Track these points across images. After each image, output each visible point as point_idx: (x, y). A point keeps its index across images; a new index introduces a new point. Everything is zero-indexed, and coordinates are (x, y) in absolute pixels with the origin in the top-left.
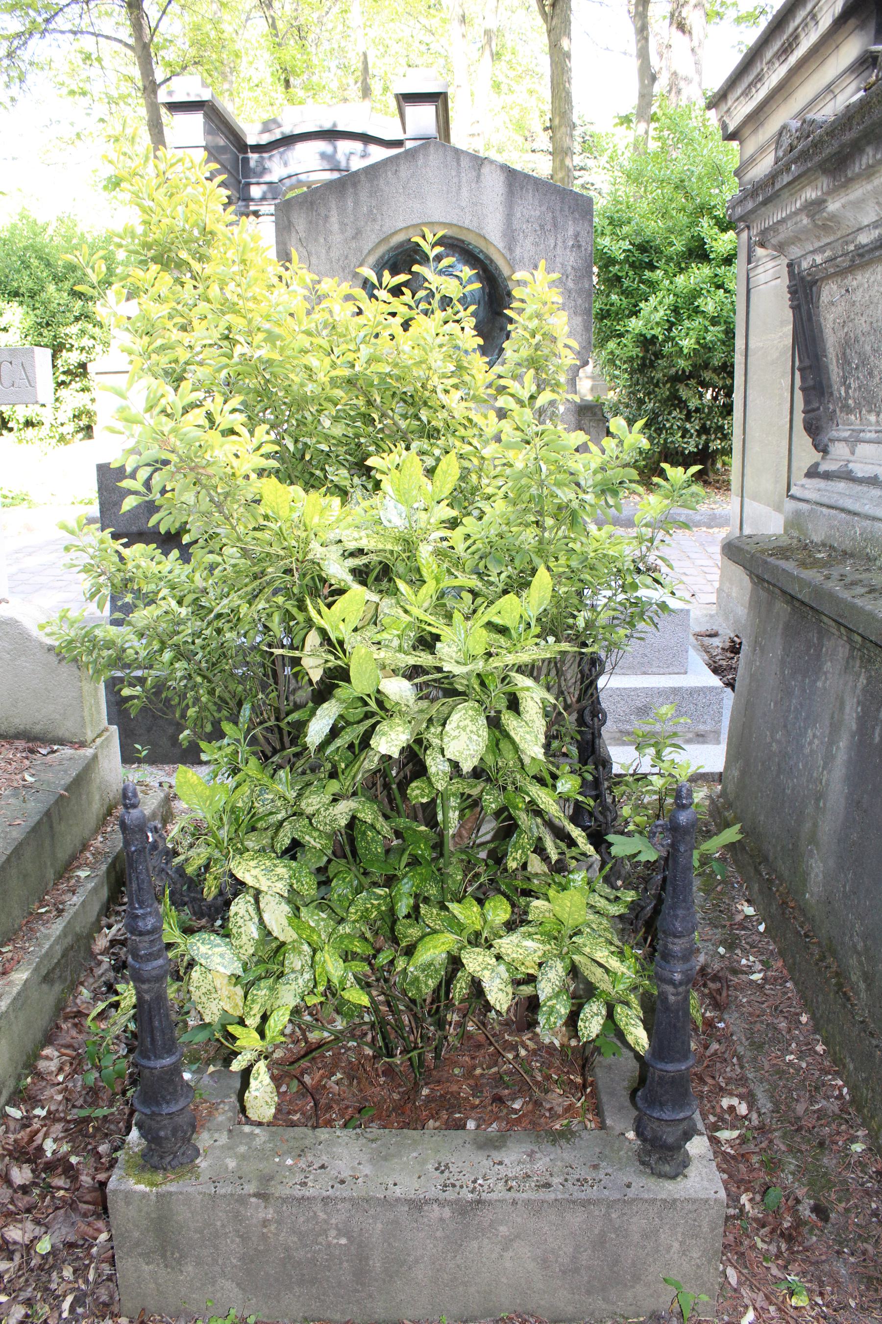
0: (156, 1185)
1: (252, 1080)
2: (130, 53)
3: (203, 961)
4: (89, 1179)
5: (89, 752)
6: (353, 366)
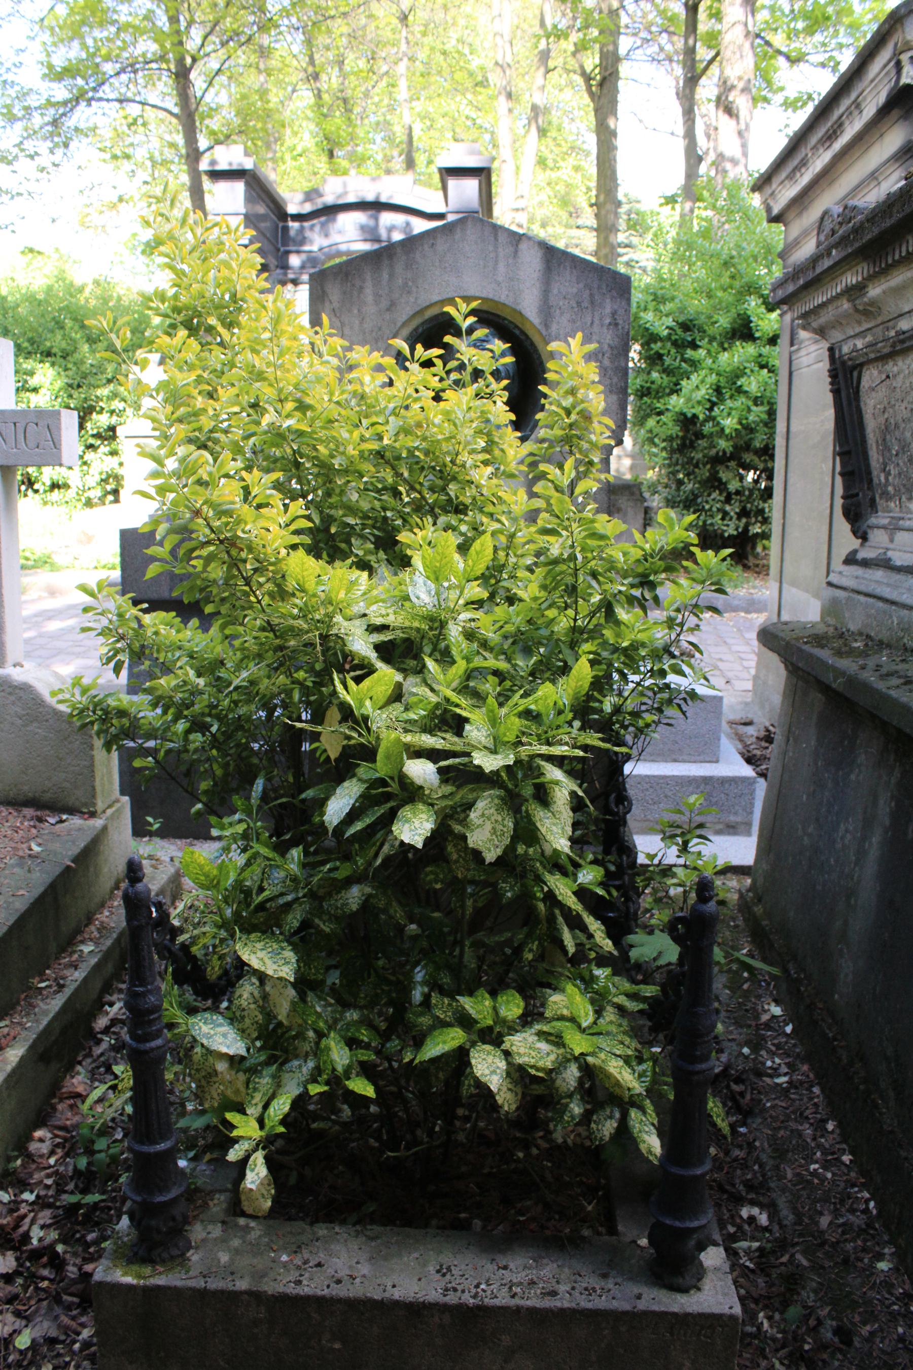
0: (144, 1278)
1: (248, 1172)
2: (174, 121)
3: (205, 1042)
4: (75, 1269)
5: (98, 823)
6: (380, 438)
